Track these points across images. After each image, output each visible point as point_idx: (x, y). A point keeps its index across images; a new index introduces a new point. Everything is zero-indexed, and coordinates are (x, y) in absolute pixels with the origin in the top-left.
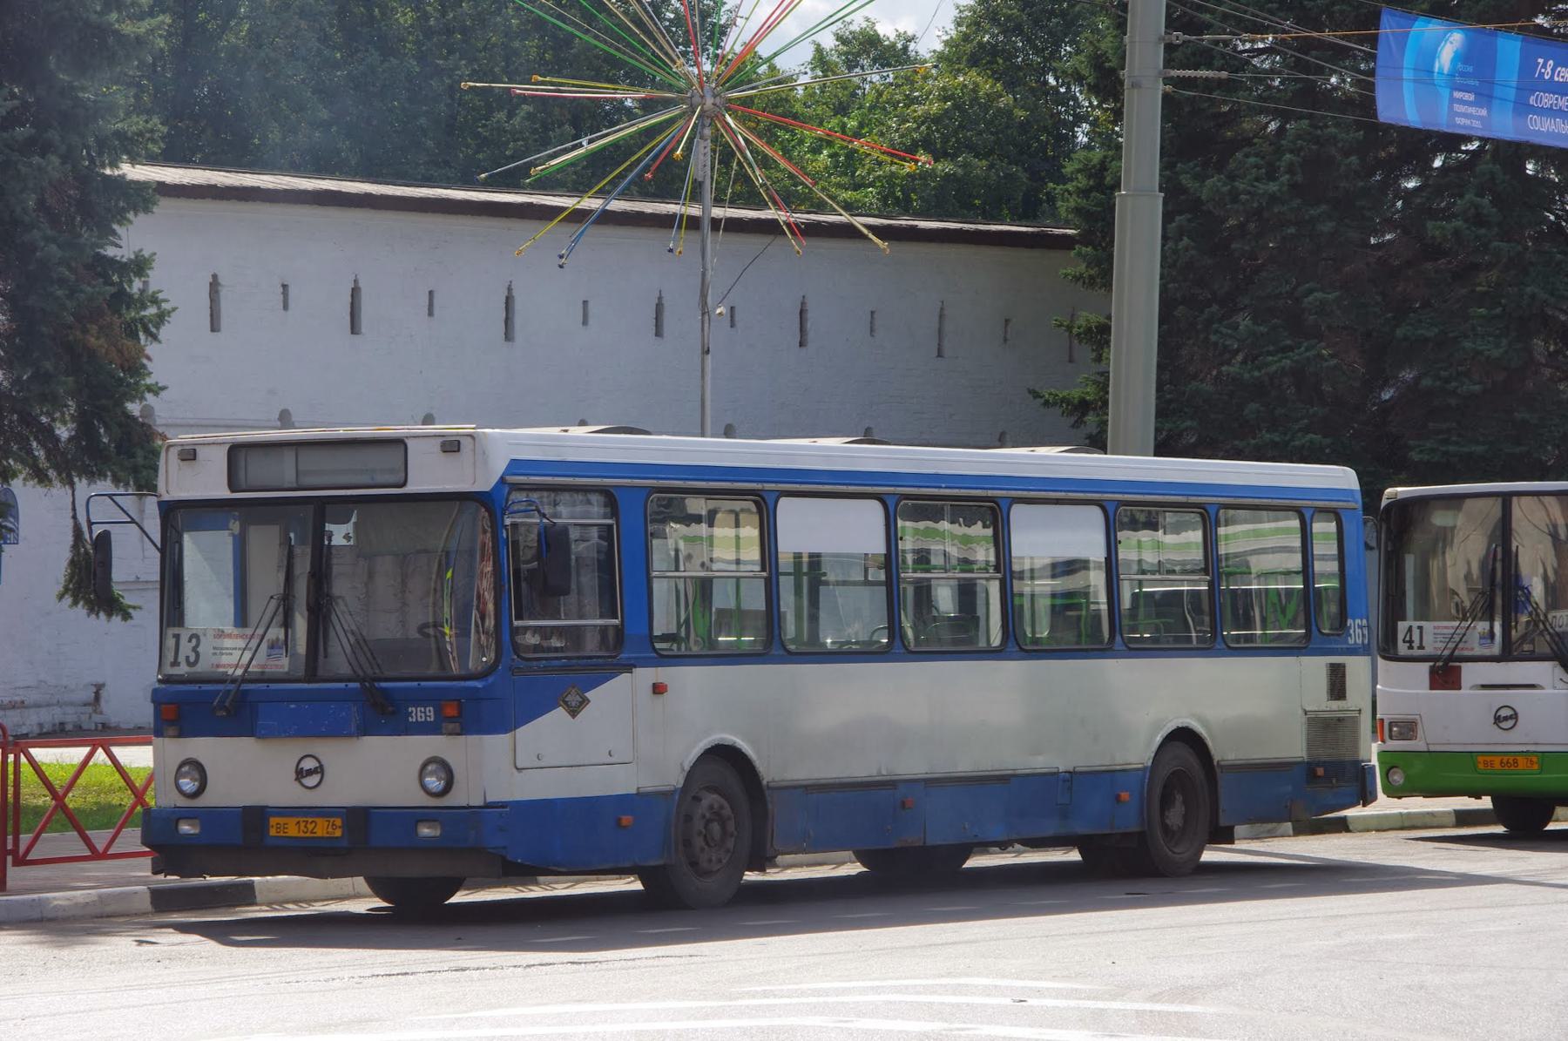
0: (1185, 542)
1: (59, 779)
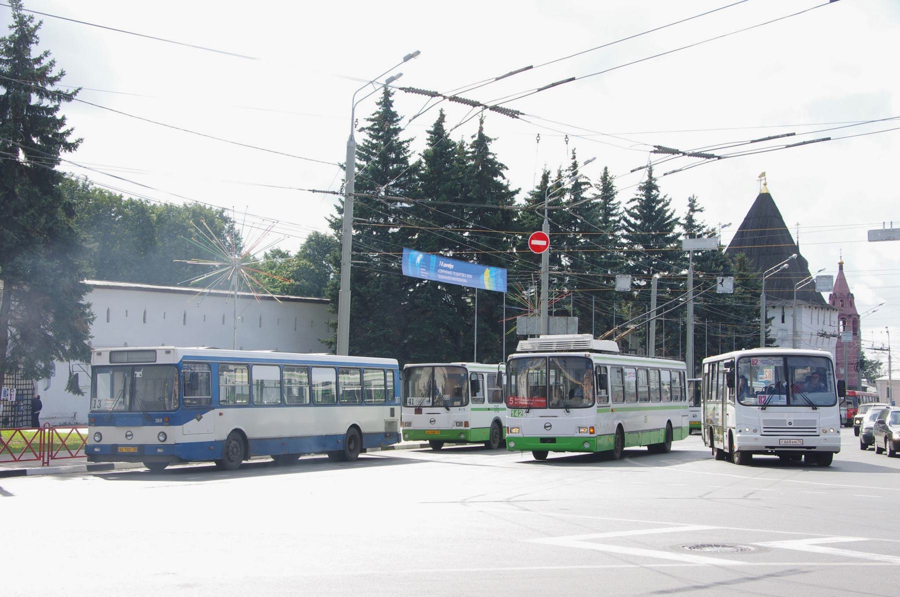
0: (355, 378)
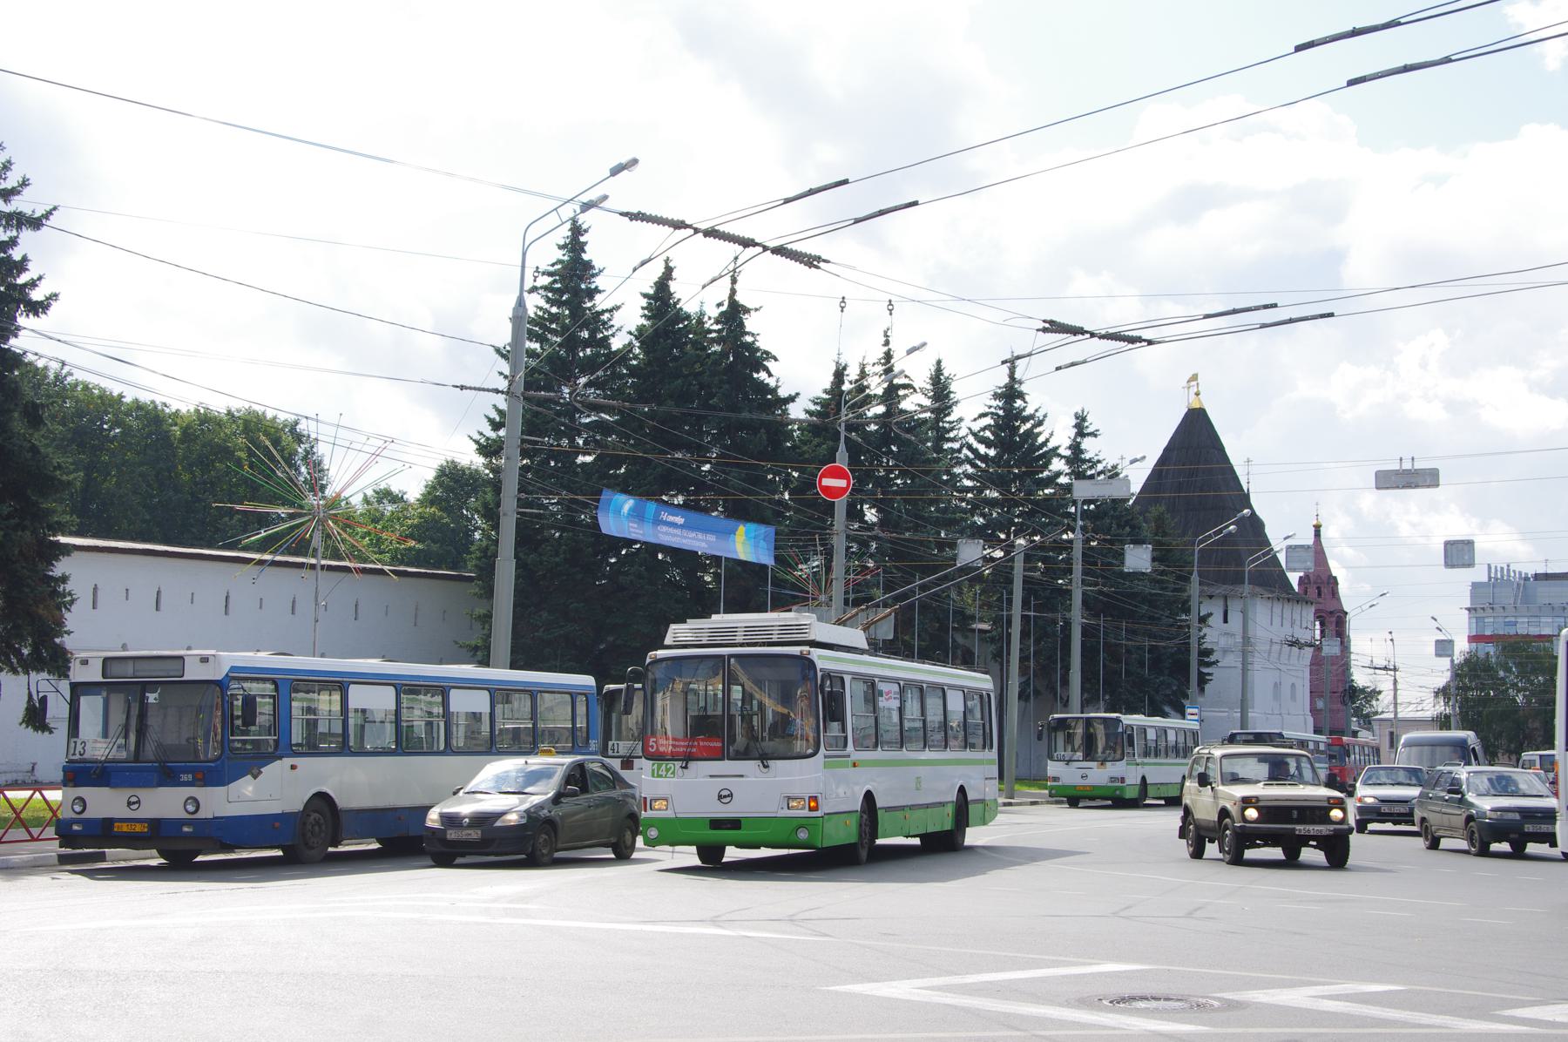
1: (18, 806)
